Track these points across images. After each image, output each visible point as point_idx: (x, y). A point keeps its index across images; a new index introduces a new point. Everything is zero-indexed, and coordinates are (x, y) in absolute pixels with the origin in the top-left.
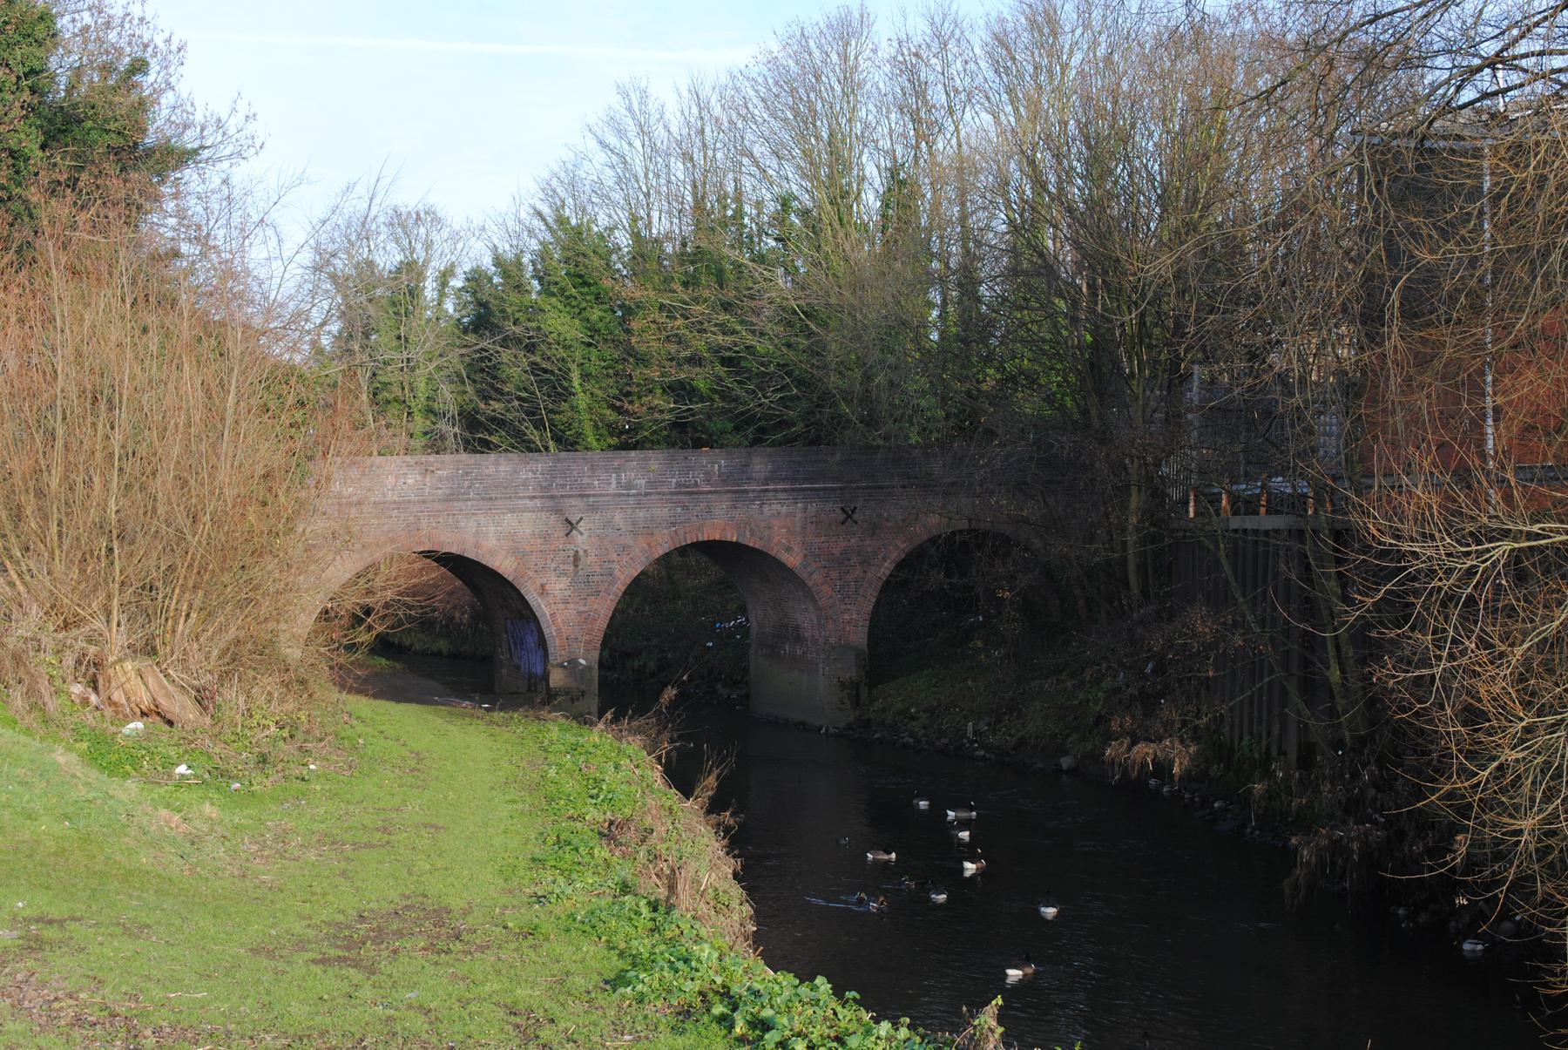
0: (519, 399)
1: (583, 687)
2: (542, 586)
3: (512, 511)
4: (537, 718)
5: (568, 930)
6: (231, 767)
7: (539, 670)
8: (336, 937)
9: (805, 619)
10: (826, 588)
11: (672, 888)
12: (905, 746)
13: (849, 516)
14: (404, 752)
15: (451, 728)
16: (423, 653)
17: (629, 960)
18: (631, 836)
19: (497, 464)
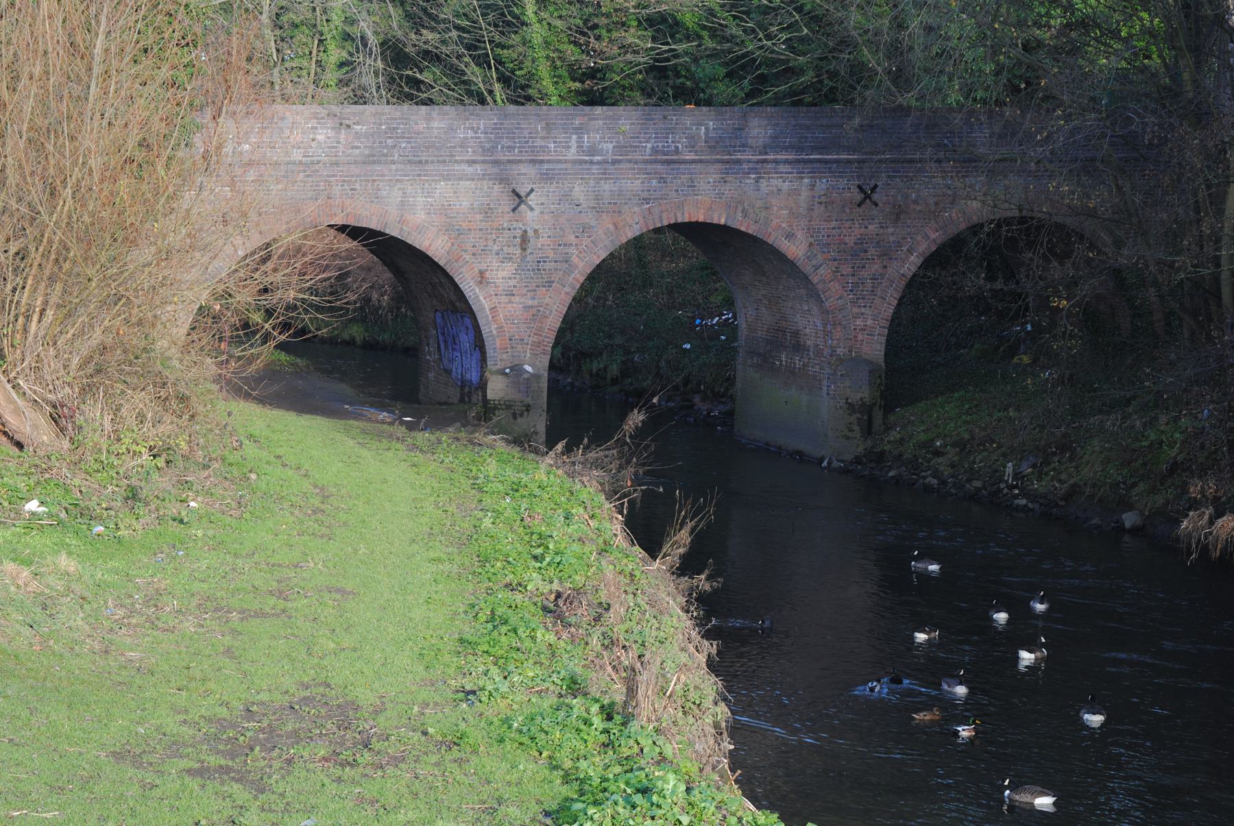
0: (458, 28)
1: (529, 400)
2: (482, 273)
3: (447, 178)
4: (471, 442)
5: (501, 741)
6: (92, 504)
7: (474, 376)
8: (217, 739)
9: (808, 323)
10: (835, 287)
11: (631, 691)
12: (927, 489)
13: (868, 197)
14: (306, 485)
15: (365, 453)
16: (331, 341)
17: (576, 786)
18: (581, 614)
19: (429, 118)
